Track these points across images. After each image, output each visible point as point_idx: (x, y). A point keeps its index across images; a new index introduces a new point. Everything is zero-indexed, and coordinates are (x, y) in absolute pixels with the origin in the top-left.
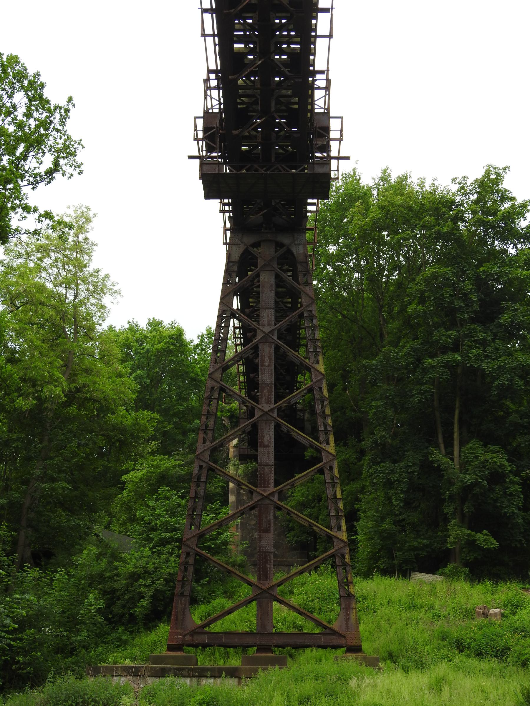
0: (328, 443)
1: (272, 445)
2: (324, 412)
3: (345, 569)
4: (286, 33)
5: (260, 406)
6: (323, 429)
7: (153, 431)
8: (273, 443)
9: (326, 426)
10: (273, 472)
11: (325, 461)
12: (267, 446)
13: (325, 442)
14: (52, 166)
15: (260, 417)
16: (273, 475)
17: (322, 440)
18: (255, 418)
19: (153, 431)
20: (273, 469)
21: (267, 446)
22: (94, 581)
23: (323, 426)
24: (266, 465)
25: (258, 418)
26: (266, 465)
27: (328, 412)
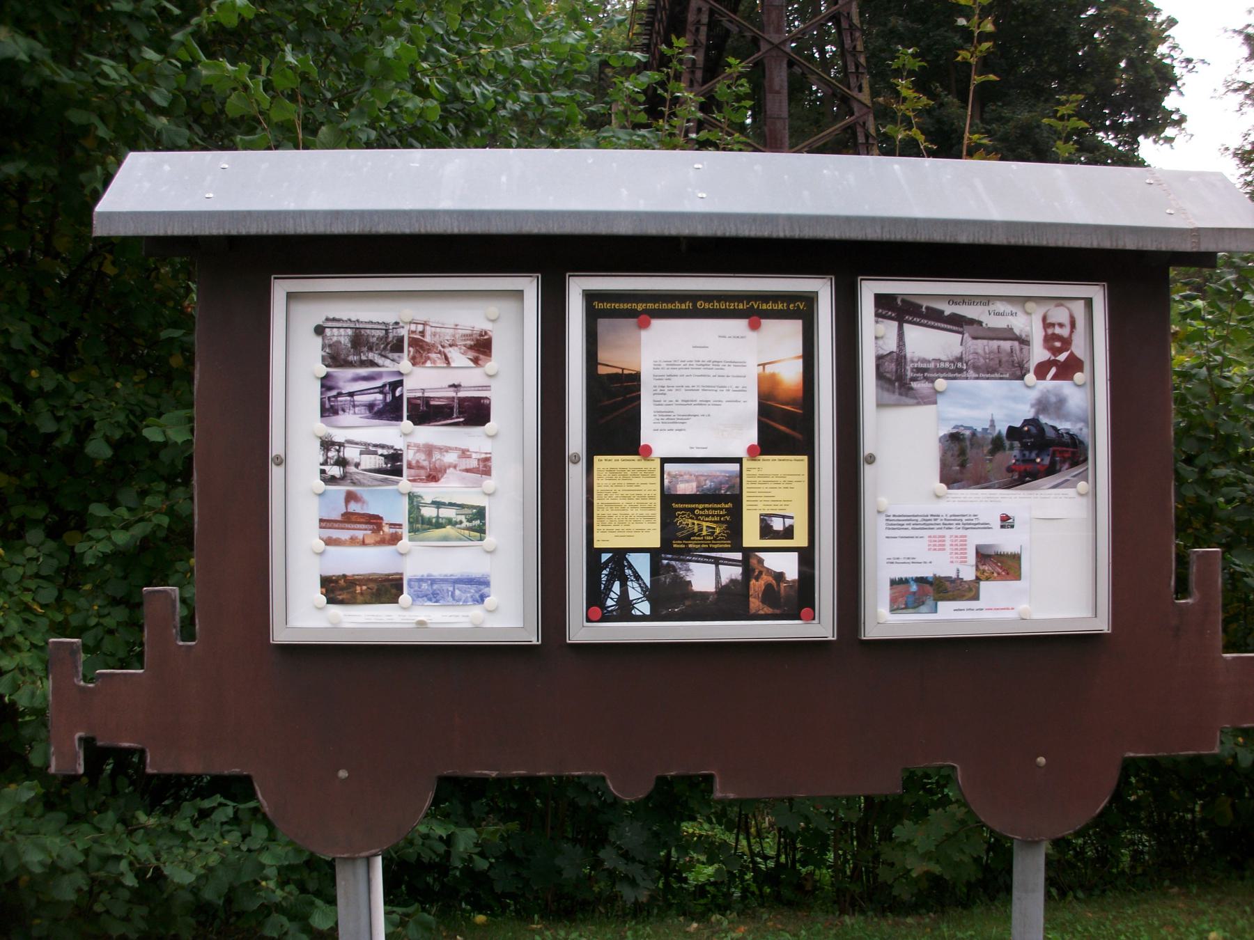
0: (860, 89)
1: (785, 91)
2: (855, 47)
3: (867, 148)
4: (855, 835)
5: (766, 36)
6: (854, 71)
7: (733, 893)
8: (786, 87)
9: (857, 65)
10: (787, 127)
11: (857, 114)
12: (778, 92)
13: (857, 89)
14: (184, 515)
15: (767, 52)
16: (787, 131)
17: (852, 85)
18: (760, 53)
19: (733, 893)
20: (787, 124)
21: (778, 92)
22: (105, 654)
23: (853, 67)
24: (778, 118)
25: (764, 53)
26: (778, 118)
27: (860, 47)
